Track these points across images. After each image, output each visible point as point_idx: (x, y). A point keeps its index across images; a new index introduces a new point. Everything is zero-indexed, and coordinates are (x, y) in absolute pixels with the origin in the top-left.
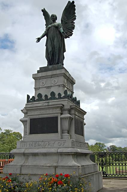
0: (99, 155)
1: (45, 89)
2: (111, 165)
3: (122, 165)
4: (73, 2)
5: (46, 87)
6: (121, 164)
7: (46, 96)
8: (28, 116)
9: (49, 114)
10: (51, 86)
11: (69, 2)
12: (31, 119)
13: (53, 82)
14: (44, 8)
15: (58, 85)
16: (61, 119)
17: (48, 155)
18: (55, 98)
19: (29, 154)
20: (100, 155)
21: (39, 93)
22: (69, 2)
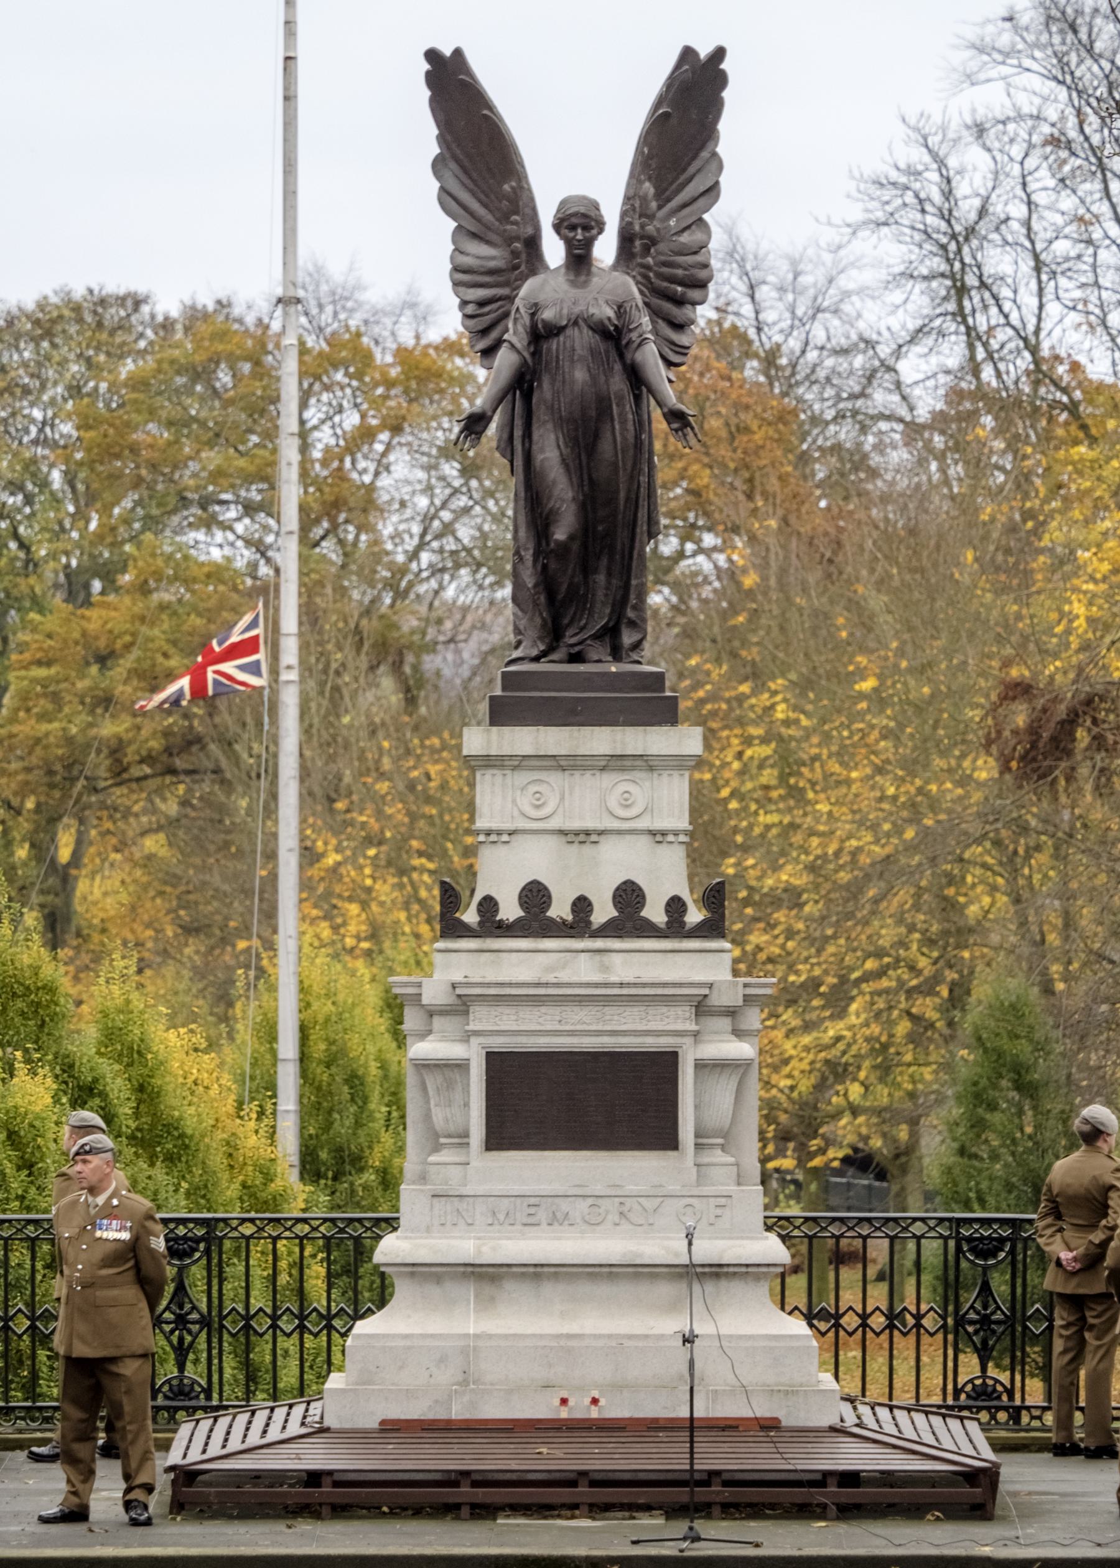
0: (959, 1240)
1: (553, 842)
2: (288, 1328)
3: (864, 1317)
4: (719, 54)
5: (562, 832)
6: (925, 1322)
7: (582, 905)
8: (477, 1033)
9: (624, 1033)
10: (601, 833)
11: (688, 53)
12: (496, 1062)
13: (525, 803)
14: (719, 54)
15: (652, 833)
16: (696, 1066)
17: (556, 1275)
18: (647, 930)
19: (444, 1269)
20: (969, 1239)
21: (625, 883)
22: (688, 53)
